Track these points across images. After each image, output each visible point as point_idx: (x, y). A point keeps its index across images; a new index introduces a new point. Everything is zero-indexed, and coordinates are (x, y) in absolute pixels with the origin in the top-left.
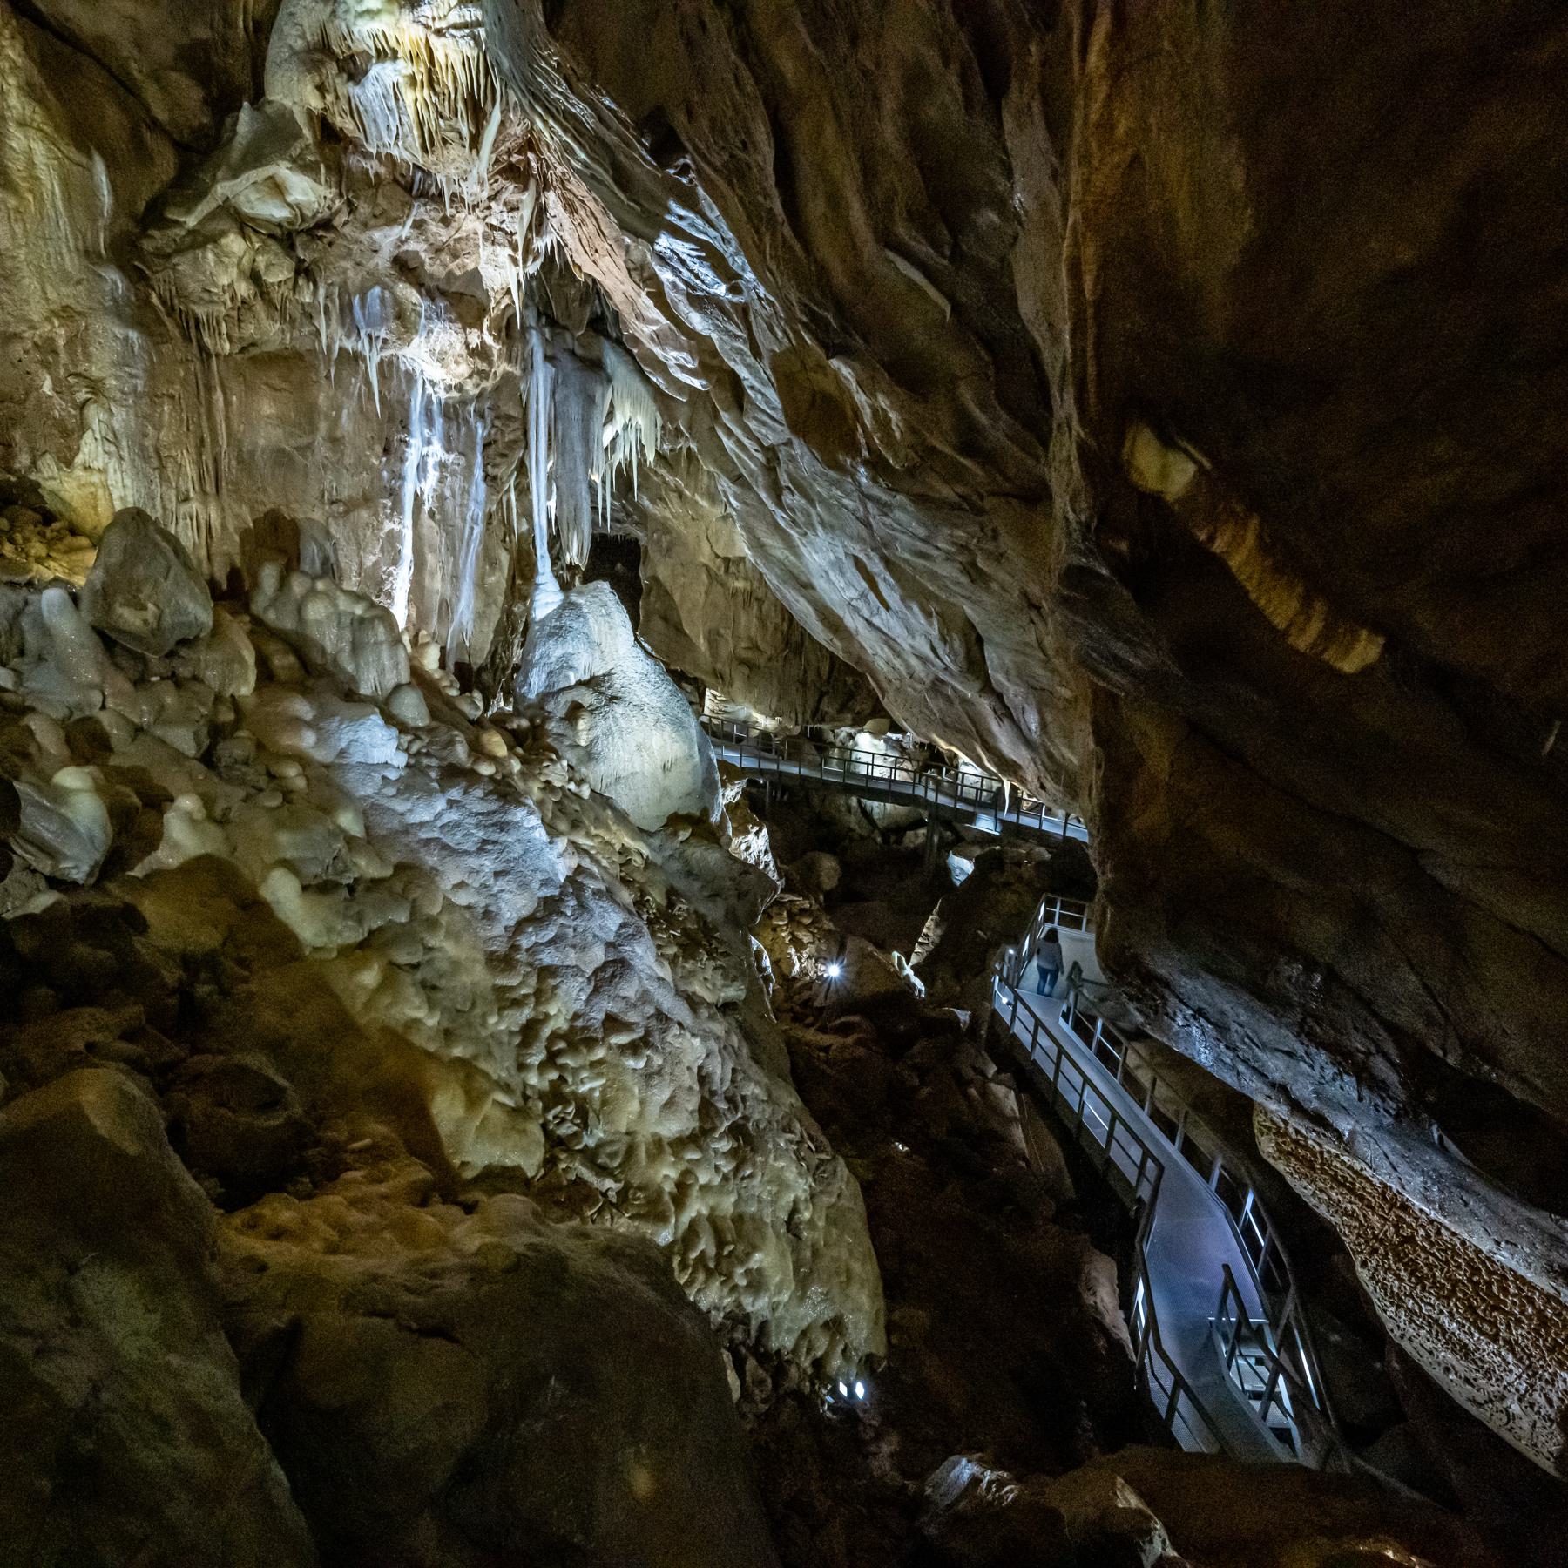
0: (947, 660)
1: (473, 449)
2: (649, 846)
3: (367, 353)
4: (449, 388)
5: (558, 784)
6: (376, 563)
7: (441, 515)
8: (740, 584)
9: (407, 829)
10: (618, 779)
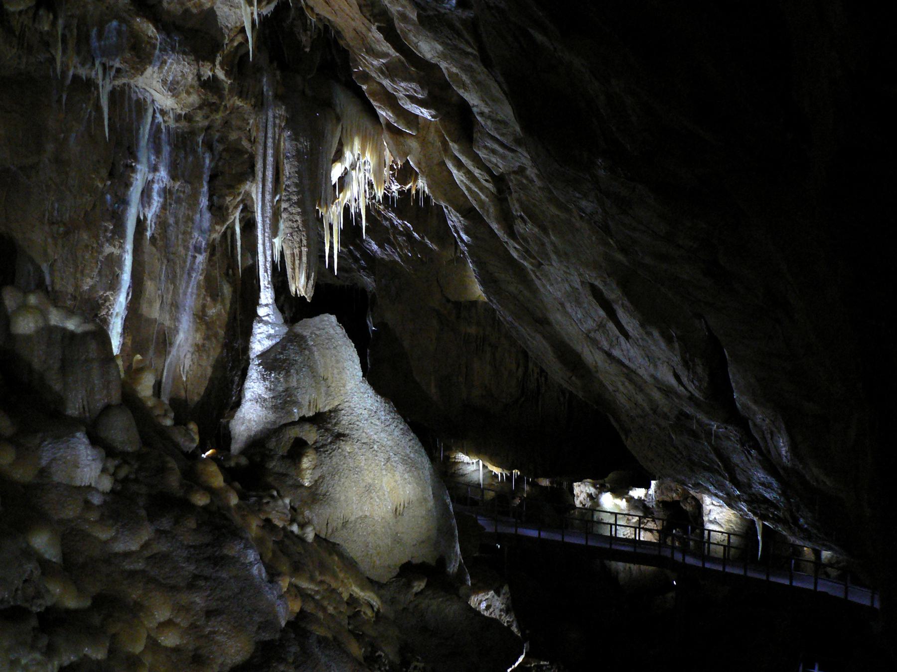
0: (691, 388)
1: (200, 178)
2: (381, 597)
3: (100, 83)
4: (178, 118)
5: (280, 524)
6: (92, 288)
7: (162, 239)
8: (472, 330)
9: (111, 559)
10: (345, 524)
